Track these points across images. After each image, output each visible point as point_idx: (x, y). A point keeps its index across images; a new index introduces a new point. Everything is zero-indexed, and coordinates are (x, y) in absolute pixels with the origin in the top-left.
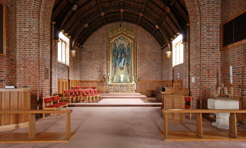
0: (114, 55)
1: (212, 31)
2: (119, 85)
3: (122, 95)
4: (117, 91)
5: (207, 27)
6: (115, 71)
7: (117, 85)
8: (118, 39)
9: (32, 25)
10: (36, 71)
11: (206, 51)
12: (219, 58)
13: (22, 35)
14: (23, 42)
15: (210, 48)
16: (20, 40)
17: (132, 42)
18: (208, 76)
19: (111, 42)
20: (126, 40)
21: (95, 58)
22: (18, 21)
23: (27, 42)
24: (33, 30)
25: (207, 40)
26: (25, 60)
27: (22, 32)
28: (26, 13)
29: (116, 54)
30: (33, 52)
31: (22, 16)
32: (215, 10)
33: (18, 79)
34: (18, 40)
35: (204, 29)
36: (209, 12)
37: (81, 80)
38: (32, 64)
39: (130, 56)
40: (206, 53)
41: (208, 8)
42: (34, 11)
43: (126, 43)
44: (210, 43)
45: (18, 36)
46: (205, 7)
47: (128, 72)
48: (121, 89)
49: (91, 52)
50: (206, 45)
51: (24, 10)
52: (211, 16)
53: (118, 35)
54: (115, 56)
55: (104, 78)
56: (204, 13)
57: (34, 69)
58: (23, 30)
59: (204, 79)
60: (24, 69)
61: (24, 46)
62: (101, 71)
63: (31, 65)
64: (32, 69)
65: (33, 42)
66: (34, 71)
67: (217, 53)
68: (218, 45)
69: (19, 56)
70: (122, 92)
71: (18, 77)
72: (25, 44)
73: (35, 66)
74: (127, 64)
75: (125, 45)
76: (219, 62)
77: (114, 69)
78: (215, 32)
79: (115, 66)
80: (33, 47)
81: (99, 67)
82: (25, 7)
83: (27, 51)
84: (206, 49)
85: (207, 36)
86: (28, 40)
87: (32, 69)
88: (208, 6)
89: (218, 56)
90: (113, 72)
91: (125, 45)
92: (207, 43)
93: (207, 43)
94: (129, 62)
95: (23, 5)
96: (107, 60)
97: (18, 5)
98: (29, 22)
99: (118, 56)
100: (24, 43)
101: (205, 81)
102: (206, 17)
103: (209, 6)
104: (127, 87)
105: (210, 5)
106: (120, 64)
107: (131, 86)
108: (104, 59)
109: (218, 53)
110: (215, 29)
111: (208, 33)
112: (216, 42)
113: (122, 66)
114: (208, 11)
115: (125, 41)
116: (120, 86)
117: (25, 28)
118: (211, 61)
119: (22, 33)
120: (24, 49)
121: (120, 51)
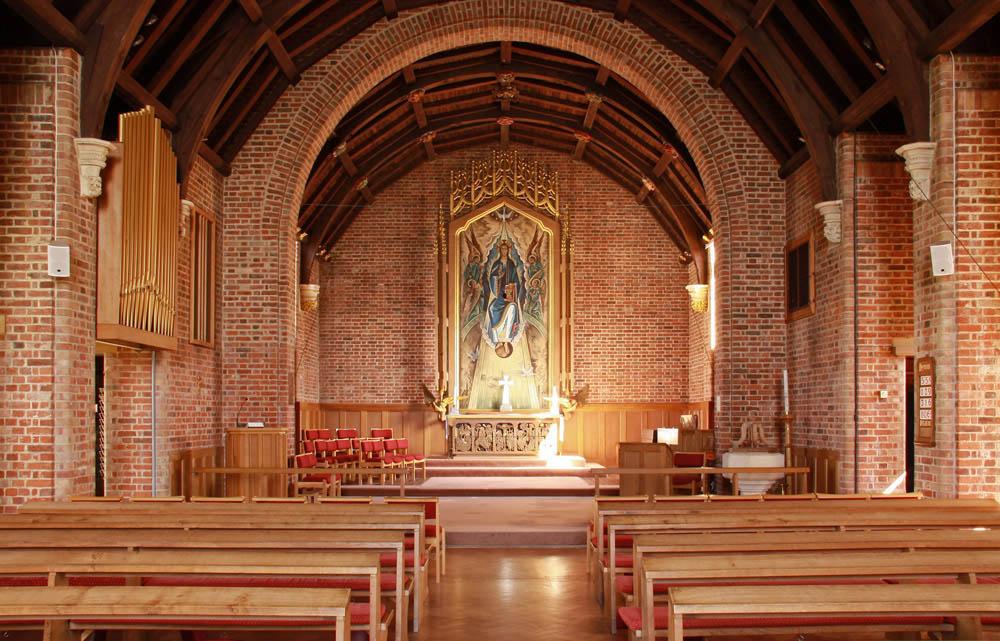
0: (469, 291)
1: (763, 267)
2: (494, 423)
3: (534, 399)
4: (488, 445)
5: (748, 256)
6: (475, 363)
7: (486, 424)
8: (488, 220)
9: (261, 258)
10: (272, 383)
11: (745, 324)
12: (782, 341)
13: (236, 284)
14: (237, 304)
15: (757, 314)
16: (231, 299)
17: (551, 233)
18: (752, 393)
19: (458, 232)
20: (524, 225)
21: (386, 304)
22: (227, 247)
23: (248, 304)
24: (265, 271)
25: (749, 292)
26: (244, 352)
27: (237, 276)
28: (247, 227)
29: (480, 288)
30: (264, 330)
31: (237, 233)
32: (769, 206)
33: (225, 404)
34: (226, 299)
35: (739, 261)
36: (752, 212)
37: (324, 401)
38: (262, 362)
39: (542, 293)
40: (747, 327)
41: (749, 201)
42: (268, 220)
43: (525, 239)
44: (757, 299)
45: (227, 288)
46: (741, 199)
47: (534, 366)
48: (503, 440)
49: (366, 279)
50: (746, 305)
51: (241, 219)
52: (760, 225)
53: (488, 202)
54: (472, 297)
55: (429, 394)
56: (739, 216)
57: (266, 377)
58: (239, 271)
59: (741, 403)
60: (242, 377)
61: (241, 316)
62: (413, 360)
63: (259, 366)
64: (261, 377)
65: (264, 304)
66: (266, 382)
67: (778, 327)
68: (779, 305)
69: (228, 342)
70: (505, 451)
71: (227, 399)
72: (243, 310)
73: (269, 369)
74: (530, 328)
75: (519, 245)
76: (783, 355)
77: (468, 353)
78: (772, 270)
79: (474, 340)
80: (263, 316)
81: (402, 343)
82: (244, 211)
83: (249, 327)
84: (746, 316)
85: (749, 281)
86: (251, 299)
87: (261, 377)
88: (750, 196)
89: (781, 336)
90: (466, 366)
91: (519, 245)
92: (749, 299)
93: (749, 299)
94: (535, 322)
95: (239, 205)
96: (440, 316)
97: (226, 205)
98: (255, 249)
99: (486, 296)
100: (240, 307)
101: (743, 409)
102: (746, 227)
103: (753, 196)
104: (529, 430)
105: (756, 193)
106: (494, 332)
107: (542, 425)
108: (426, 309)
109: (781, 329)
110: (771, 261)
111: (751, 272)
112: (774, 296)
113: (507, 339)
114: (749, 211)
115: (520, 228)
116: (498, 429)
117: (244, 266)
118: (761, 350)
119: (236, 279)
120: (240, 324)
121: (495, 273)
